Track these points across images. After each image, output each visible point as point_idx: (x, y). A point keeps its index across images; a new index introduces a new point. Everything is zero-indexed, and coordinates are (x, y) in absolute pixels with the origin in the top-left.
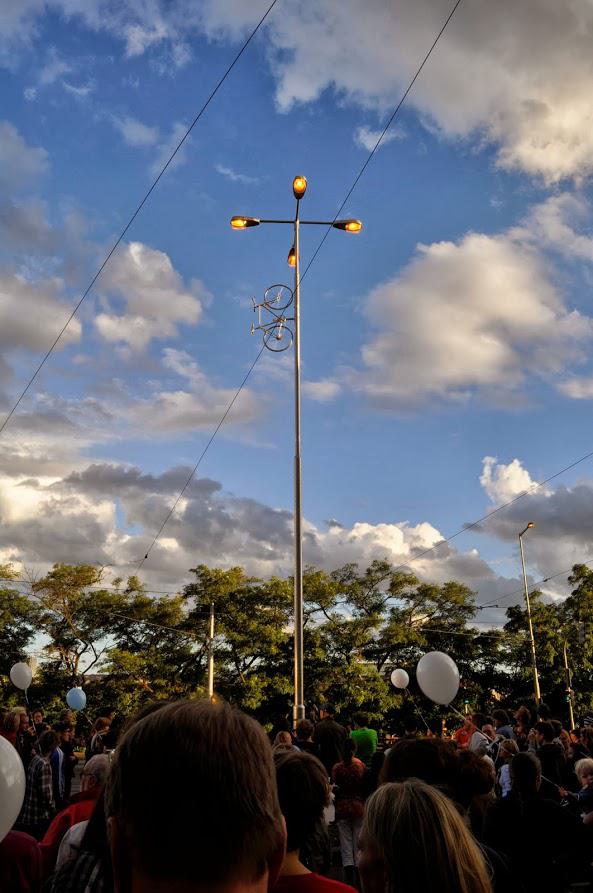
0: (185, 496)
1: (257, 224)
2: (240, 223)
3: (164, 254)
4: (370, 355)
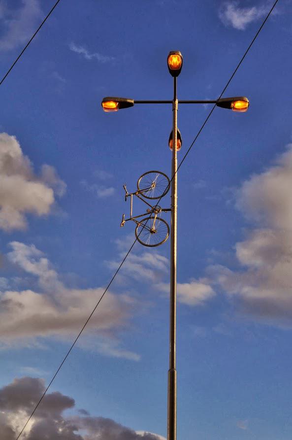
0: (32, 414)
1: (131, 105)
2: (113, 105)
3: (13, 138)
4: (244, 253)
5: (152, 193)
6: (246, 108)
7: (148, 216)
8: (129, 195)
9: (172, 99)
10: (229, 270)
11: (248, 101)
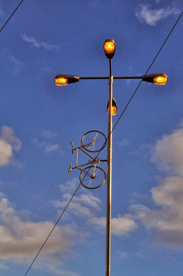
1: (77, 80)
2: (63, 80)
5: (92, 148)
6: (165, 82)
7: (90, 165)
8: (75, 149)
9: (108, 76)
10: (147, 208)
11: (167, 77)
